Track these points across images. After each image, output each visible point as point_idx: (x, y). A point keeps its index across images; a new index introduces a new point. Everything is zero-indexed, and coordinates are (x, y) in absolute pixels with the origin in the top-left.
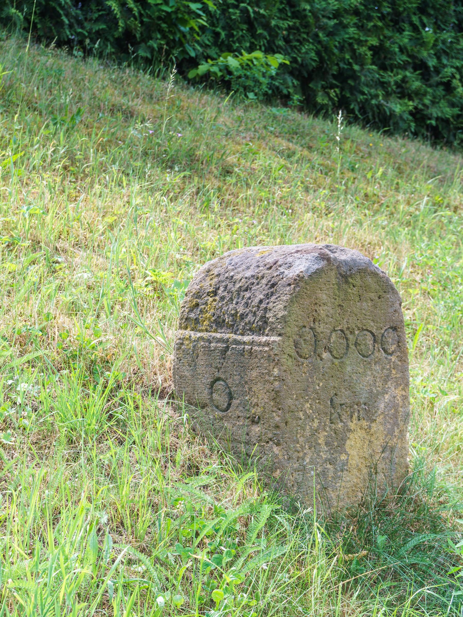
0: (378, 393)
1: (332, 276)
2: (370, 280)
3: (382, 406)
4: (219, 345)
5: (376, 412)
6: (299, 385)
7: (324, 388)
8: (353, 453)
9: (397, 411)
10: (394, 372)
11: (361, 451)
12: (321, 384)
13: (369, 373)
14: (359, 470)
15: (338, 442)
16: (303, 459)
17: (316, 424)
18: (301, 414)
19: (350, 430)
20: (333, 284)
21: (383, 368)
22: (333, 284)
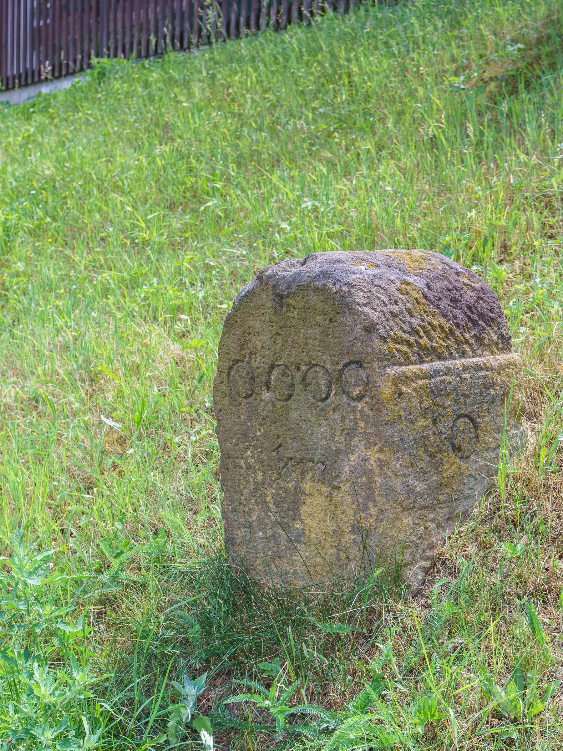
0: (339, 452)
1: (267, 300)
2: (314, 299)
3: (347, 469)
4: (309, 241)
5: (337, 476)
6: (237, 428)
7: (266, 435)
8: (312, 523)
9: (371, 480)
10: (362, 425)
11: (322, 523)
12: (262, 430)
13: (325, 423)
14: (471, 489)
15: (291, 505)
16: (249, 515)
17: (260, 477)
18: (242, 461)
19: (303, 493)
20: (268, 308)
21: (343, 419)
22: (268, 308)
